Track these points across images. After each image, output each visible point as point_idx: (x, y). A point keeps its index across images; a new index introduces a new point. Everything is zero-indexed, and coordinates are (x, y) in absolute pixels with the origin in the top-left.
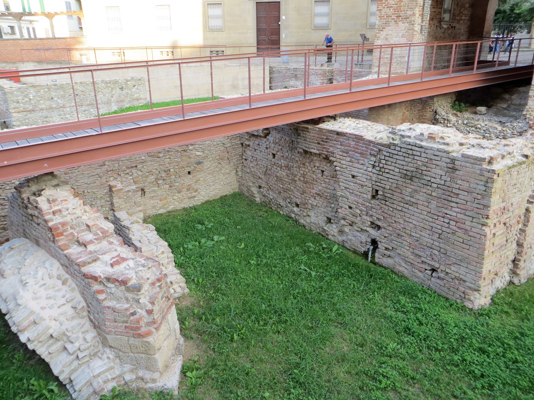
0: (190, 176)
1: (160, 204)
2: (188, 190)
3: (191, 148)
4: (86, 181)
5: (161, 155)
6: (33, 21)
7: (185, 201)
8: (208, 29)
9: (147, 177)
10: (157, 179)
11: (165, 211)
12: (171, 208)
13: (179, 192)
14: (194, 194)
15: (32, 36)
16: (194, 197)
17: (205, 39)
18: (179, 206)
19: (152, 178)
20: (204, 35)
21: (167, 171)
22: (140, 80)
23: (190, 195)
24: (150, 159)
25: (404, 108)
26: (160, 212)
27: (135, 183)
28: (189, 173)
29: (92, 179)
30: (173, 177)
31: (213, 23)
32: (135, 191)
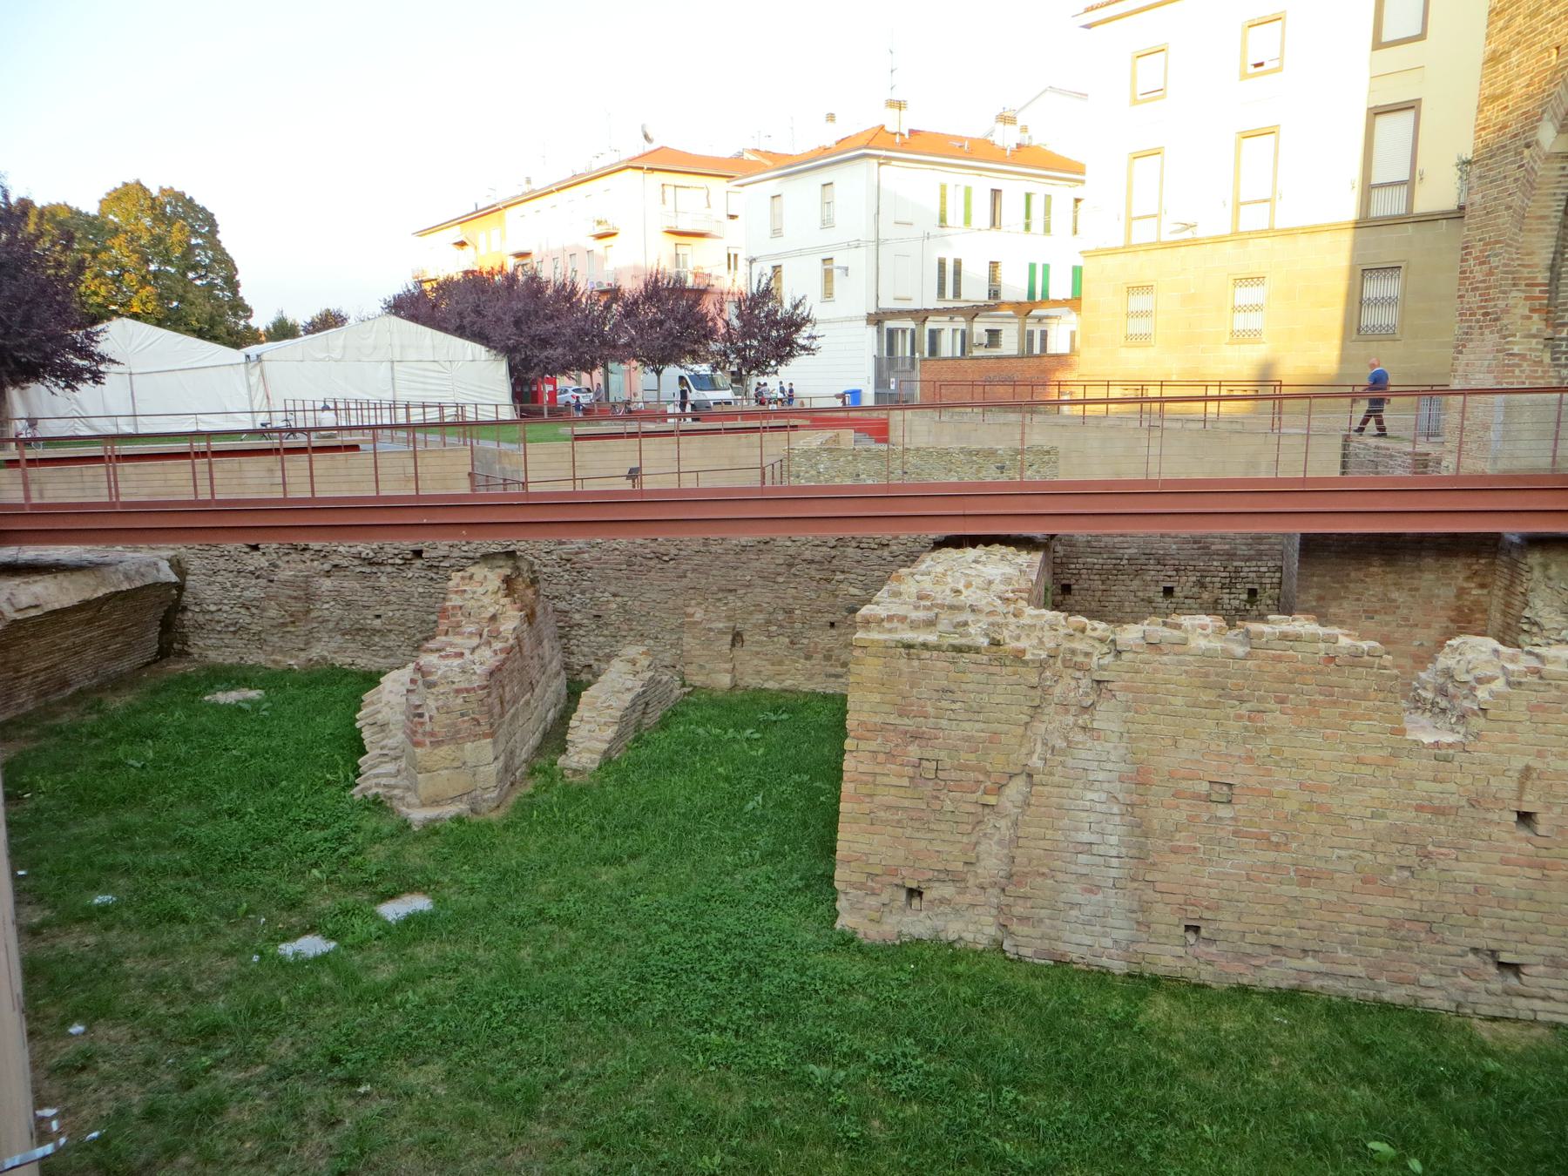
0: (833, 632)
1: (768, 669)
2: (828, 658)
3: (840, 577)
4: (654, 596)
5: (781, 579)
6: (1047, 317)
7: (818, 679)
8: (1355, 331)
9: (751, 613)
10: (768, 622)
11: (777, 686)
12: (788, 683)
13: (808, 658)
14: (839, 670)
15: (1037, 350)
16: (838, 676)
17: (1344, 359)
18: (807, 687)
19: (760, 618)
20: (1344, 348)
21: (789, 612)
22: (1048, 452)
23: (832, 670)
24: (761, 582)
25: (1461, 577)
26: (766, 685)
27: (729, 618)
28: (832, 625)
29: (663, 596)
30: (798, 625)
31: (1372, 317)
32: (721, 632)
